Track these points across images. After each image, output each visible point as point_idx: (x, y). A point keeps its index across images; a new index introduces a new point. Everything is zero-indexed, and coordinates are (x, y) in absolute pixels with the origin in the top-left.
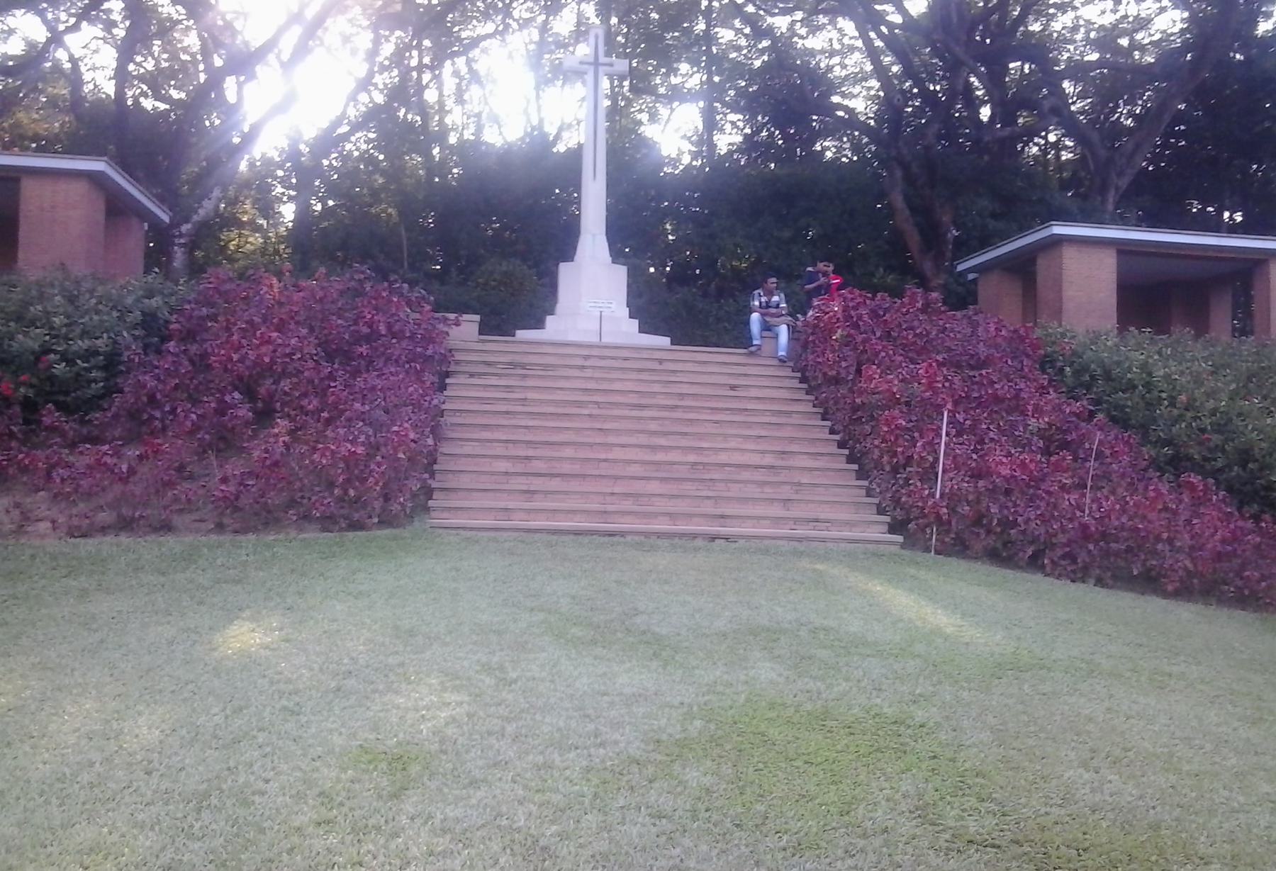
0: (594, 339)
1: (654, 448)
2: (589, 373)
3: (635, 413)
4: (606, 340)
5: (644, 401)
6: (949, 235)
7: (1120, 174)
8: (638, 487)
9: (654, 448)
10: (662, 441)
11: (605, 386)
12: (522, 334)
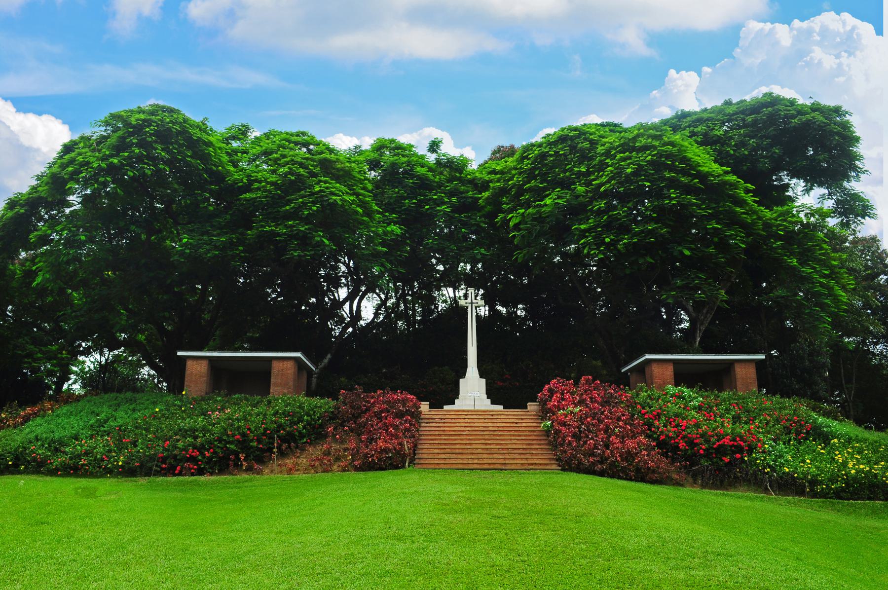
0: (472, 409)
1: (486, 444)
2: (466, 421)
3: (482, 433)
4: (477, 408)
5: (484, 429)
6: (621, 357)
7: (702, 324)
8: (480, 456)
9: (486, 444)
10: (489, 442)
11: (472, 425)
12: (446, 407)
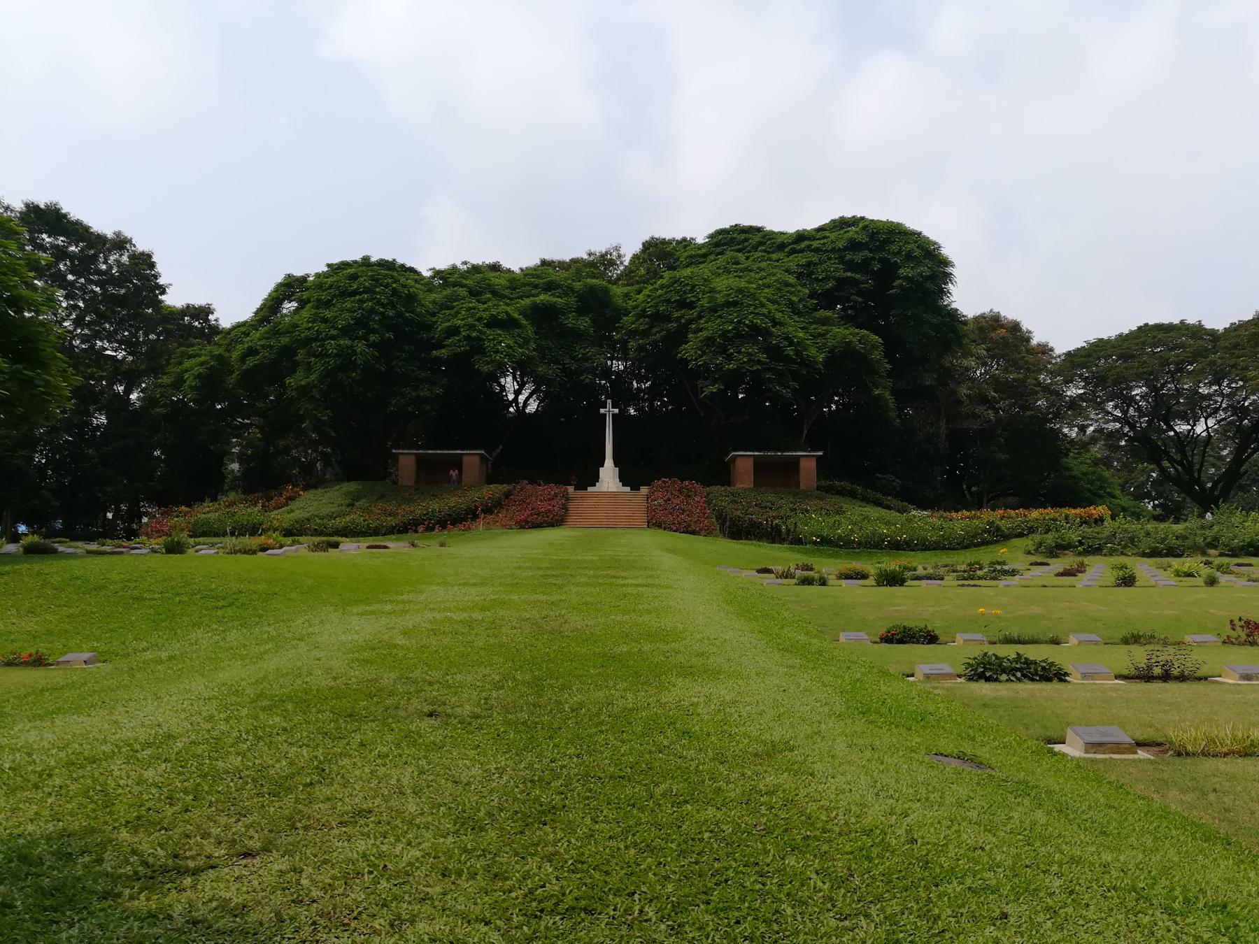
0: (606, 490)
